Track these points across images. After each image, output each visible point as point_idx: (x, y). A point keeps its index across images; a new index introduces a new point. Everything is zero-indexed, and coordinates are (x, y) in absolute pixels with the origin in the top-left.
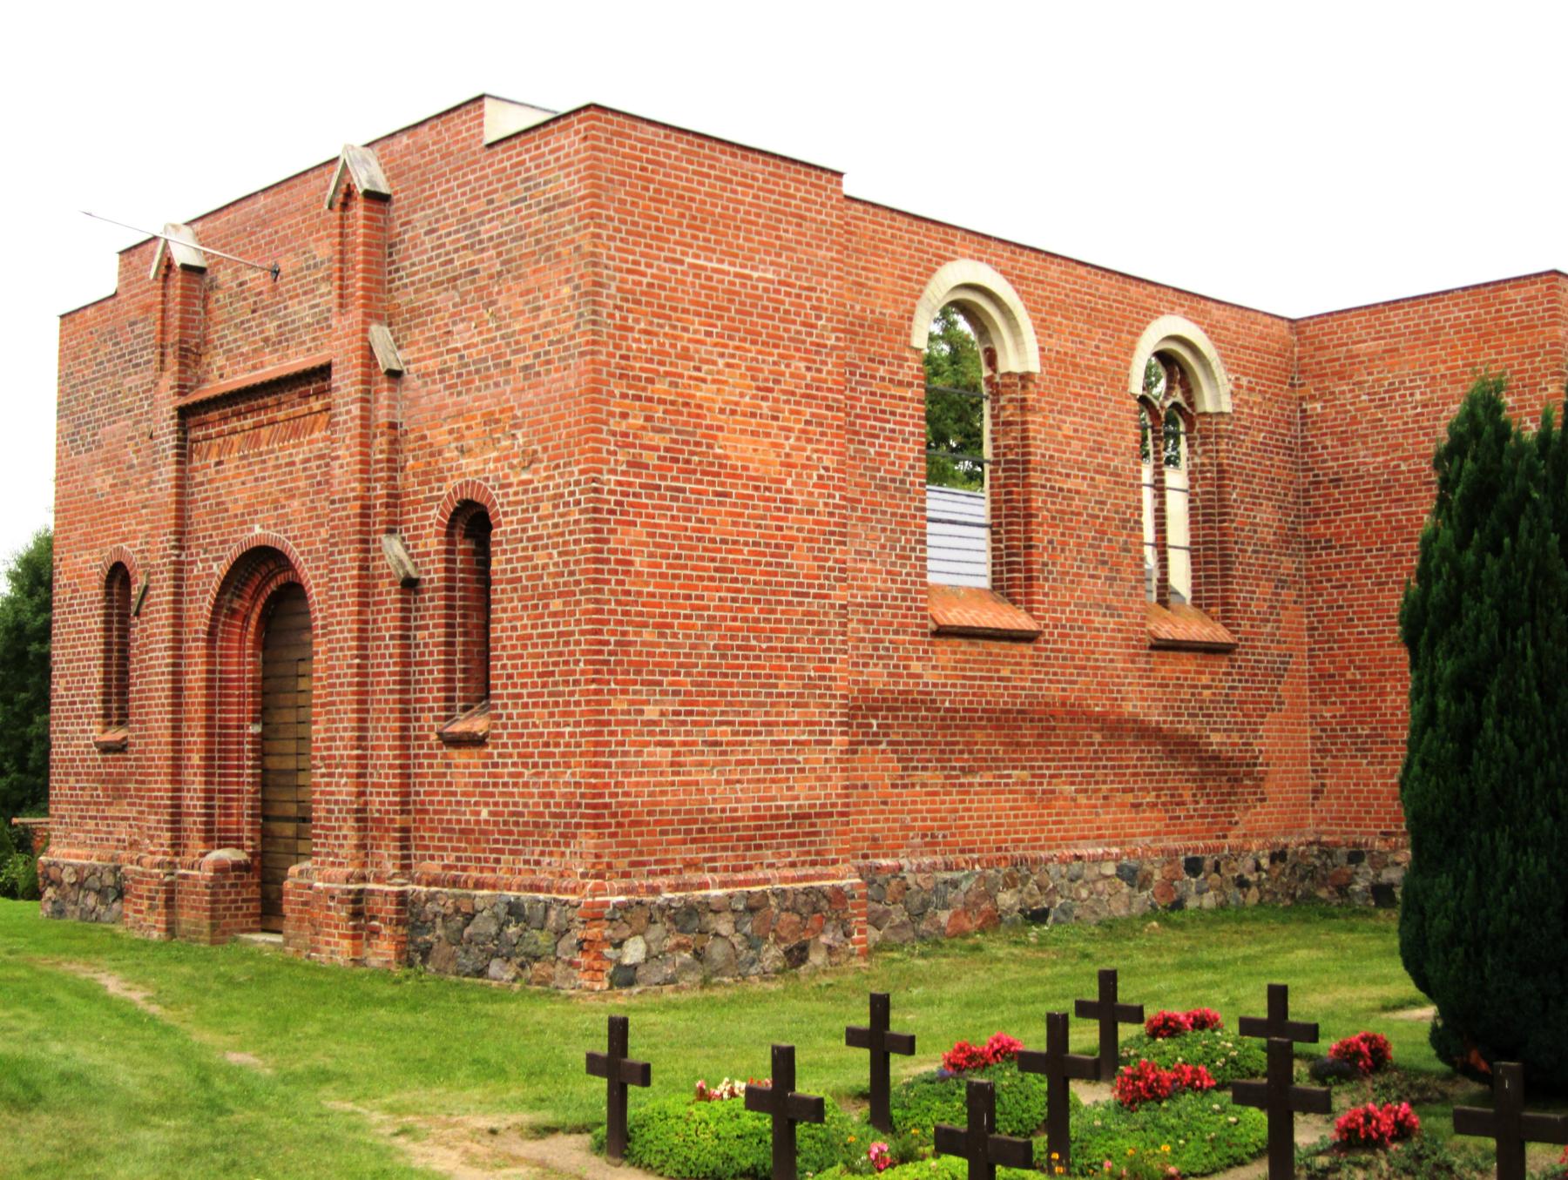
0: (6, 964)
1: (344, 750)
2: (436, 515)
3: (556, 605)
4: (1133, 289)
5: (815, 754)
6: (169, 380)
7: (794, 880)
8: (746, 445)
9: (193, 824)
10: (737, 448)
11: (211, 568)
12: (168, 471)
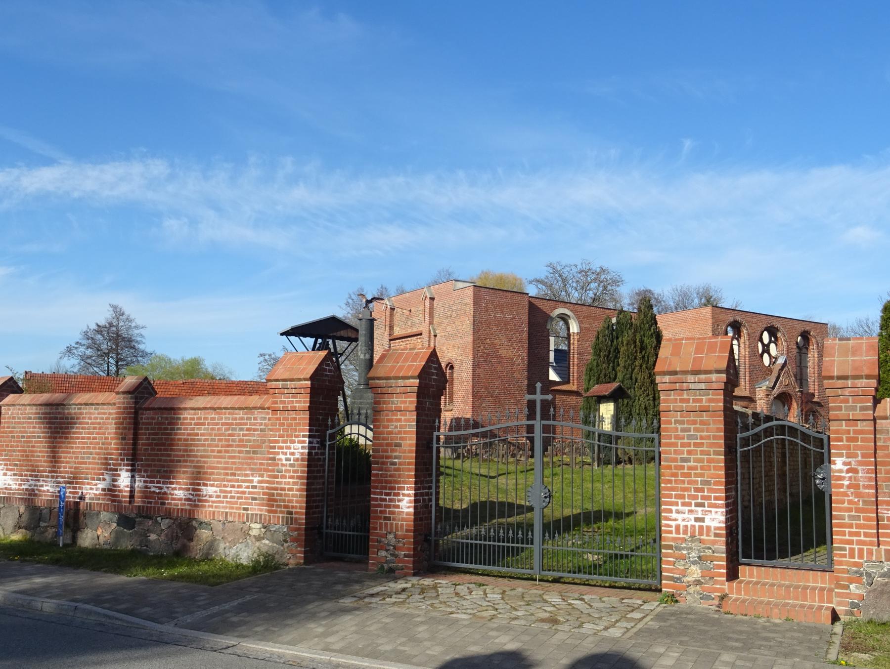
6: (387, 333)
8: (505, 352)
10: (504, 352)
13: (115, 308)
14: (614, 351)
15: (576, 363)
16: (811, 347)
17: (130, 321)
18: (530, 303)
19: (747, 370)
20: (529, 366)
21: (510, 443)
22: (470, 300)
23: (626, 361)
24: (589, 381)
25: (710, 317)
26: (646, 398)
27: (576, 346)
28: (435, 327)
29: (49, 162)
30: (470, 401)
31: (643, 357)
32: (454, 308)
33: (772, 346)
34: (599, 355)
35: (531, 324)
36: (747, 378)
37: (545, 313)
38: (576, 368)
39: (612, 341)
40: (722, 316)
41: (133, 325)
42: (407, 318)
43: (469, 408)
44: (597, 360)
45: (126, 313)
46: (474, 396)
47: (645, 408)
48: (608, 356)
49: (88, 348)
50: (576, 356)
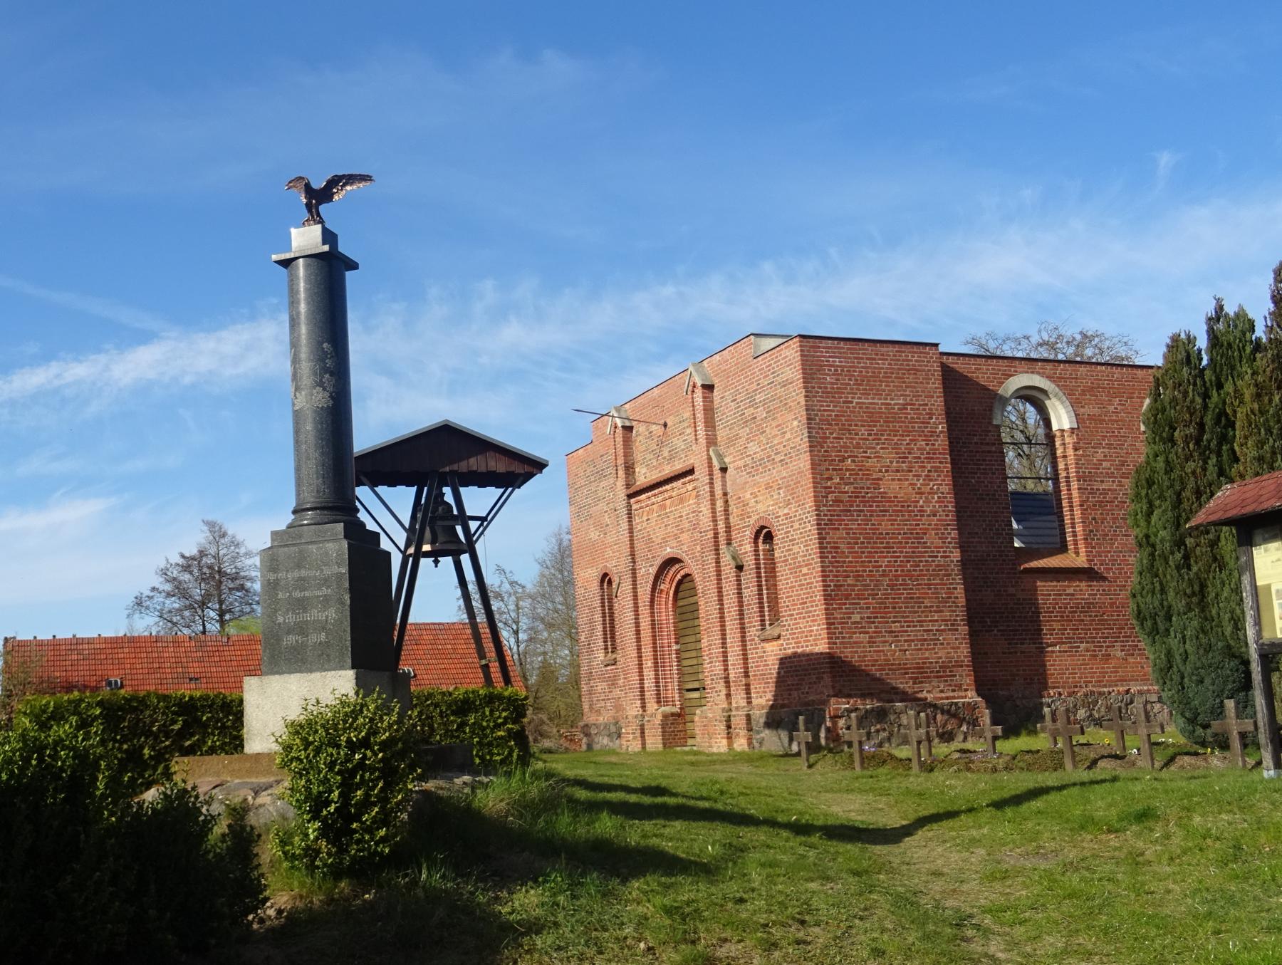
2: (749, 533)
3: (805, 570)
4: (1139, 372)
5: (951, 637)
6: (621, 482)
7: (942, 698)
8: (895, 486)
9: (650, 695)
10: (891, 487)
11: (647, 571)
12: (625, 526)
13: (211, 525)
14: (1218, 422)
17: (237, 545)
20: (959, 517)
21: (935, 706)
23: (1260, 445)
24: (1149, 514)
27: (1071, 460)
28: (722, 449)
29: (145, 338)
30: (819, 610)
32: (758, 398)
34: (1171, 440)
37: (985, 388)
38: (1077, 512)
39: (1206, 396)
41: (242, 550)
42: (661, 443)
45: (230, 532)
46: (828, 598)
48: (1198, 441)
49: (169, 595)
50: (1074, 485)
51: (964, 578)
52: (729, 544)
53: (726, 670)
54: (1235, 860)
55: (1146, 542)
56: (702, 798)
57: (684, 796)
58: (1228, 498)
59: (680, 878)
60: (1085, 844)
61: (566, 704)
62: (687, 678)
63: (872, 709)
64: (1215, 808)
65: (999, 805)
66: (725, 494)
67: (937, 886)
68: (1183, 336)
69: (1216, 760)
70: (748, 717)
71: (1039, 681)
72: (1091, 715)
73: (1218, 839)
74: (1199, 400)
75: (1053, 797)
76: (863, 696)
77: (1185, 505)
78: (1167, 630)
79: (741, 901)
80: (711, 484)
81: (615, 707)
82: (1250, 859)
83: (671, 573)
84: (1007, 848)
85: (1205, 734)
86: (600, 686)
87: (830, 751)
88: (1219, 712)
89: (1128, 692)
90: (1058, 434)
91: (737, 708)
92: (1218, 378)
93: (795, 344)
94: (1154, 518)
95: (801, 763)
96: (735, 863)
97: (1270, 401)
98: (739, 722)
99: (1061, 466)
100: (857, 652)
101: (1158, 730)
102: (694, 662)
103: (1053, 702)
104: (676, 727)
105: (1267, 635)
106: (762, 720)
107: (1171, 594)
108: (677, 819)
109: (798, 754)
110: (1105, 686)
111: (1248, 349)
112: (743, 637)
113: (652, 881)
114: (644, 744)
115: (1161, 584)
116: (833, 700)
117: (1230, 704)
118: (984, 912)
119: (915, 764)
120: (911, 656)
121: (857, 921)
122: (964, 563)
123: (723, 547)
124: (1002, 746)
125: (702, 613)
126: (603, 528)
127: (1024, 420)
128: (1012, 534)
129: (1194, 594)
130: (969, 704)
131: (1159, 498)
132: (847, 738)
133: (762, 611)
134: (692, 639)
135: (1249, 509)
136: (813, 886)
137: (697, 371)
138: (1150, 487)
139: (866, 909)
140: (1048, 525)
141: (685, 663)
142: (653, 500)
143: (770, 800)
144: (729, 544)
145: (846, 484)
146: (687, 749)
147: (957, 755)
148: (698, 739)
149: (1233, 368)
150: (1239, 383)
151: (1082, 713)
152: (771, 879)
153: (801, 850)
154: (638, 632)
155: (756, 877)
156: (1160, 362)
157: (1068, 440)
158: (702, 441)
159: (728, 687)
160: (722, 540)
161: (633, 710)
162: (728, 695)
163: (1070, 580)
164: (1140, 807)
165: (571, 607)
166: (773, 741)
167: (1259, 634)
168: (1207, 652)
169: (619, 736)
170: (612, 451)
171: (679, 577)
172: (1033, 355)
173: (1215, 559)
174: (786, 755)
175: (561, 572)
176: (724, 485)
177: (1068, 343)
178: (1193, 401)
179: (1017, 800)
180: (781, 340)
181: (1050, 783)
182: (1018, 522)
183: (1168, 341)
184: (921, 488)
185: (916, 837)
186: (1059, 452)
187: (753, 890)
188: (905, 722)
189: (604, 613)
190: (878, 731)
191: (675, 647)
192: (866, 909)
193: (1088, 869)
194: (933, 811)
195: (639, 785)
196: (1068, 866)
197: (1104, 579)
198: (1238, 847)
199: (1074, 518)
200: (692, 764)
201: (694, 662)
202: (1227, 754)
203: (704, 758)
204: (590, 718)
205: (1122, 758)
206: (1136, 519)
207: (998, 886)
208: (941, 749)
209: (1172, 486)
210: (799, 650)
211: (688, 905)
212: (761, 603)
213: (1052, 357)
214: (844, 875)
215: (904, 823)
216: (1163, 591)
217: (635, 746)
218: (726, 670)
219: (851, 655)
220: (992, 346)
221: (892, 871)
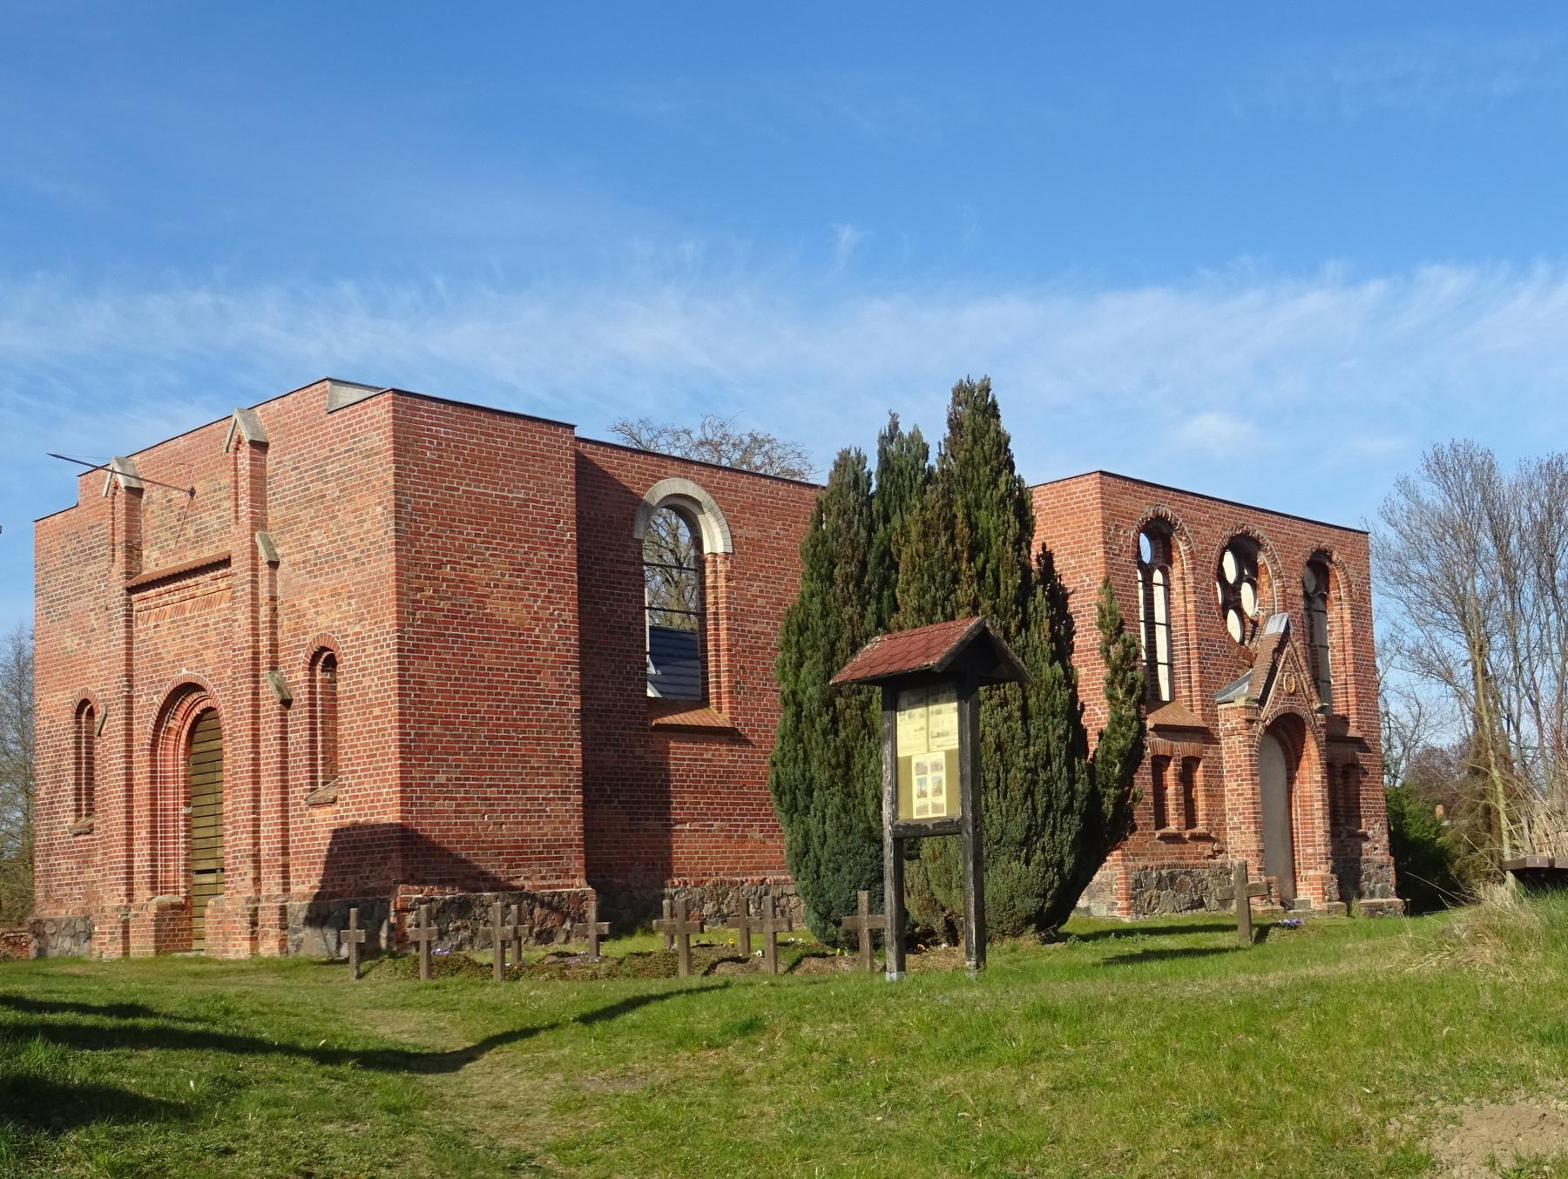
0: (6, 958)
1: (245, 817)
2: (303, 657)
3: (377, 711)
5: (558, 807)
6: (119, 568)
7: (543, 887)
8: (505, 606)
10: (500, 607)
11: (150, 701)
12: (121, 632)
14: (881, 561)
15: (724, 644)
16: (1333, 594)
18: (578, 455)
19: (1194, 654)
20: (583, 655)
21: (533, 897)
22: (380, 439)
23: (923, 592)
24: (799, 666)
25: (1097, 503)
26: (1001, 714)
28: (273, 536)
30: (392, 767)
31: (981, 575)
32: (330, 469)
33: (1246, 589)
34: (830, 578)
35: (586, 526)
36: (1195, 677)
37: (627, 491)
38: (724, 659)
39: (871, 529)
40: (1127, 503)
42: (183, 518)
43: (390, 792)
44: (823, 593)
46: (405, 751)
47: (999, 747)
50: (723, 624)
51: (583, 733)
52: (274, 669)
53: (256, 844)
54: (839, 1077)
55: (793, 700)
56: (196, 1019)
57: (165, 1016)
58: (879, 653)
59: (141, 1126)
60: (680, 1064)
61: (12, 892)
62: (198, 855)
63: (453, 901)
64: (827, 1016)
65: (587, 1019)
66: (273, 599)
67: (497, 1122)
68: (853, 454)
69: (844, 963)
70: (283, 909)
71: (662, 867)
72: (719, 910)
73: (825, 1052)
74: (863, 533)
75: (653, 1009)
76: (442, 883)
77: (839, 658)
78: (807, 807)
79: (228, 1151)
80: (254, 582)
81: (86, 895)
82: (854, 1073)
83: (186, 705)
84: (589, 1072)
85: (837, 934)
86: (65, 865)
87: (393, 956)
88: (852, 907)
89: (762, 882)
90: (710, 558)
91: (268, 898)
92: (886, 510)
93: (386, 401)
94: (804, 671)
95: (350, 972)
96: (226, 1103)
97: (937, 542)
98: (269, 916)
99: (710, 599)
100: (441, 823)
101: (785, 927)
102: (211, 832)
103: (676, 892)
104: (177, 924)
105: (902, 815)
106: (302, 915)
107: (815, 763)
108: (150, 1047)
109: (346, 961)
110: (738, 875)
111: (920, 479)
112: (284, 799)
113: (100, 1131)
114: (126, 949)
115: (805, 751)
116: (401, 888)
117: (863, 896)
118: (548, 1151)
119: (497, 972)
120: (508, 832)
121: (383, 1170)
122: (584, 713)
123: (265, 673)
124: (607, 948)
125: (227, 763)
126: (87, 634)
127: (675, 537)
128: (644, 680)
129: (839, 765)
130: (576, 894)
131: (812, 647)
132: (412, 937)
133: (313, 765)
134: (210, 800)
135: (895, 668)
136: (330, 1128)
137: (244, 420)
138: (801, 633)
139: (397, 1155)
140: (691, 671)
141: (197, 833)
142: (166, 598)
143: (292, 1019)
144: (274, 669)
145: (441, 599)
146: (190, 955)
147: (554, 958)
148: (209, 941)
149: (902, 499)
150: (907, 517)
151: (709, 908)
152: (273, 1122)
153: (323, 1084)
154: (129, 787)
155: (253, 1119)
156: (825, 482)
157: (720, 567)
158: (246, 520)
159: (257, 868)
160: (264, 663)
161: (113, 899)
162: (257, 880)
163: (709, 742)
164: (745, 1017)
165: (28, 748)
166: (316, 943)
167: (895, 813)
168: (847, 834)
169: (89, 937)
170: (108, 523)
171: (197, 711)
172: (694, 457)
173: (865, 725)
174: (331, 962)
175: (19, 695)
176: (273, 585)
177: (734, 445)
178: (857, 534)
179: (610, 1013)
180: (368, 393)
181: (654, 991)
182: (656, 665)
183: (837, 457)
184: (539, 615)
185: (480, 1062)
186: (709, 582)
187: (246, 1137)
188: (491, 916)
189: (78, 758)
190: (457, 929)
191: (184, 810)
192: (397, 1155)
193: (678, 1093)
194: (508, 1029)
195: (103, 1004)
196: (658, 1090)
197: (748, 743)
198: (843, 1061)
199: (719, 664)
200: (196, 975)
201: (211, 832)
202: (857, 956)
203: (214, 967)
204: (44, 911)
205: (744, 961)
206: (784, 673)
207: (570, 1118)
208: (535, 952)
209: (827, 633)
210: (361, 820)
211: (148, 1161)
212: (313, 753)
213: (714, 461)
214: (376, 1113)
215: (469, 1045)
216: (806, 760)
217: (113, 951)
218: (256, 844)
219: (430, 828)
220: (645, 436)
221: (443, 1105)
